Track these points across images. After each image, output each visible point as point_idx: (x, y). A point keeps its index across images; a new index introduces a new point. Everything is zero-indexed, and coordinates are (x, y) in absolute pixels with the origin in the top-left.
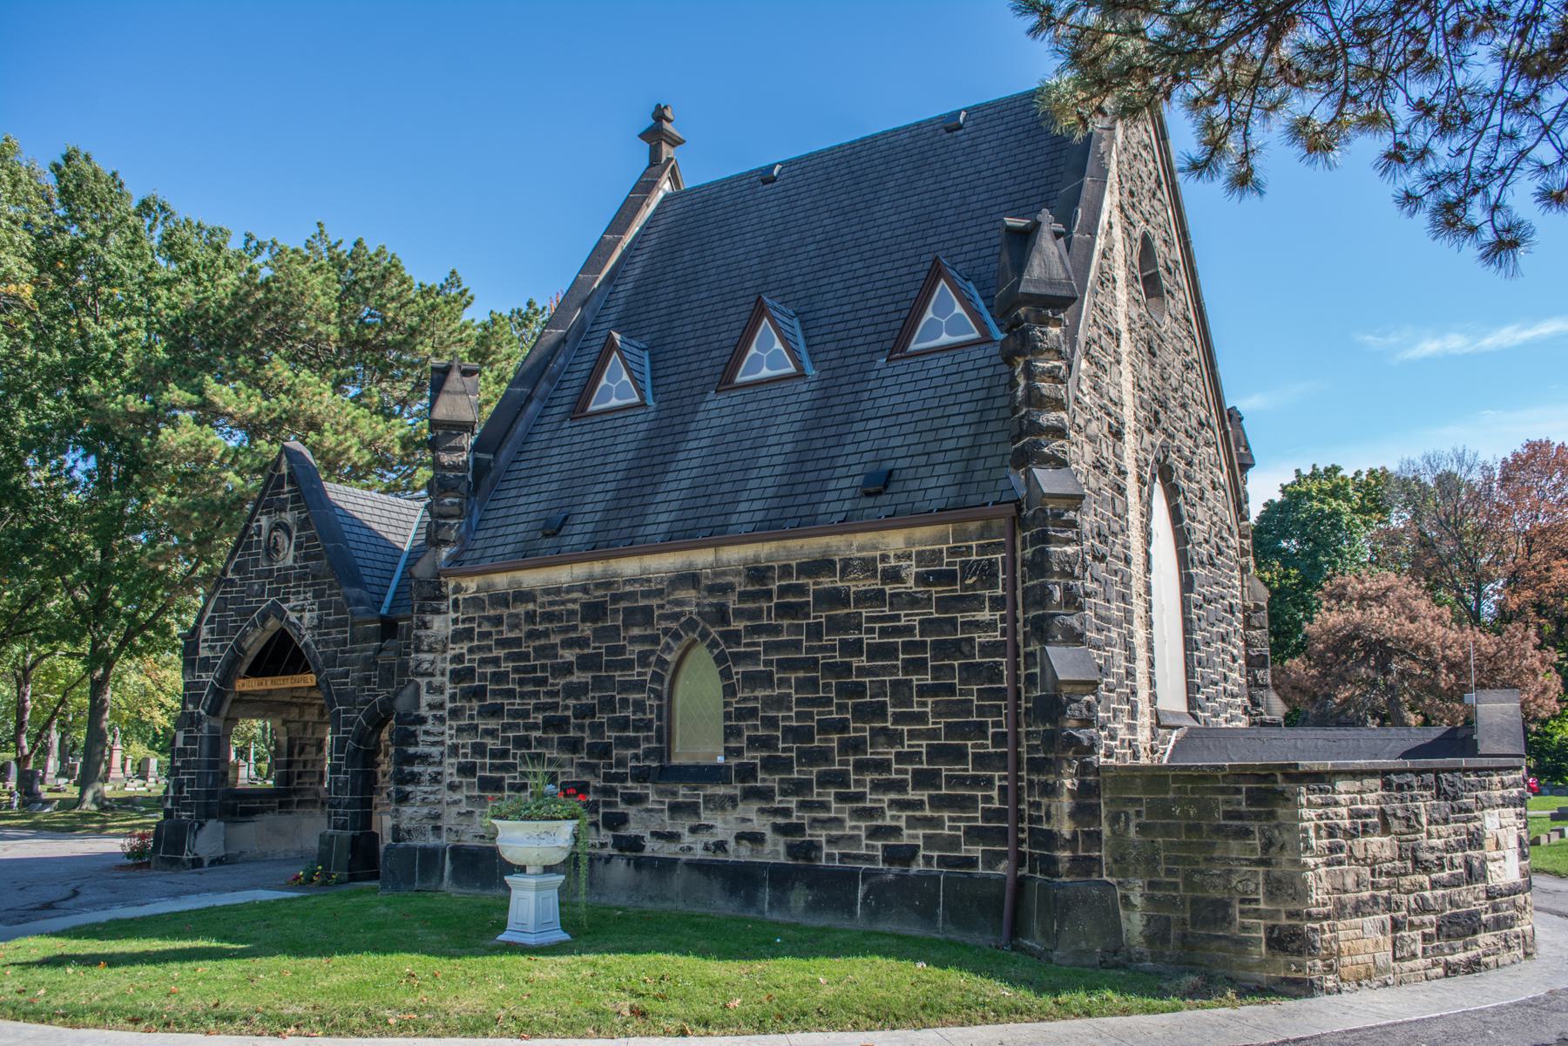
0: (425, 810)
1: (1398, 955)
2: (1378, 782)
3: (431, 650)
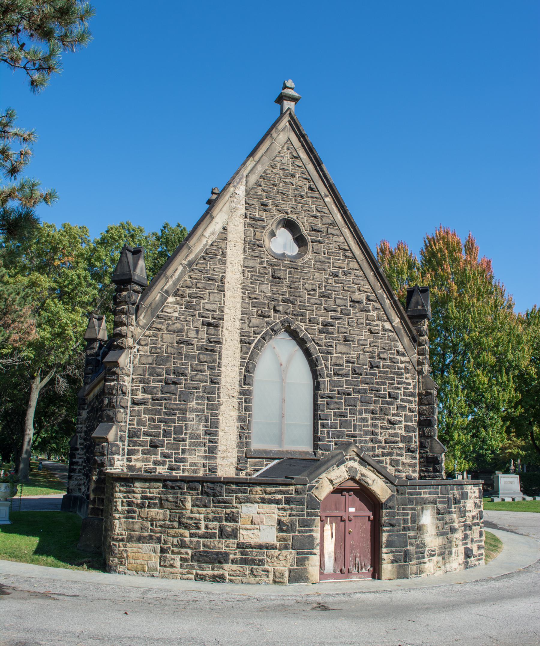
0: (76, 482)
1: (162, 564)
2: (161, 485)
3: (81, 424)
